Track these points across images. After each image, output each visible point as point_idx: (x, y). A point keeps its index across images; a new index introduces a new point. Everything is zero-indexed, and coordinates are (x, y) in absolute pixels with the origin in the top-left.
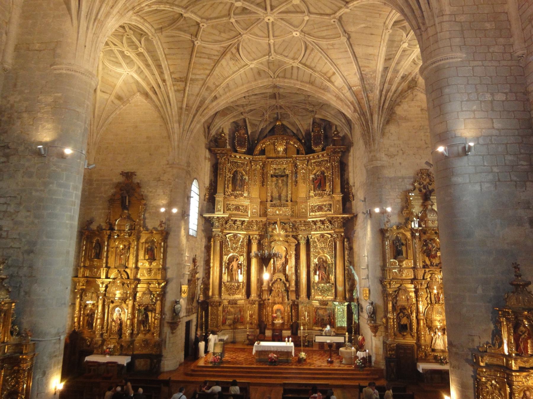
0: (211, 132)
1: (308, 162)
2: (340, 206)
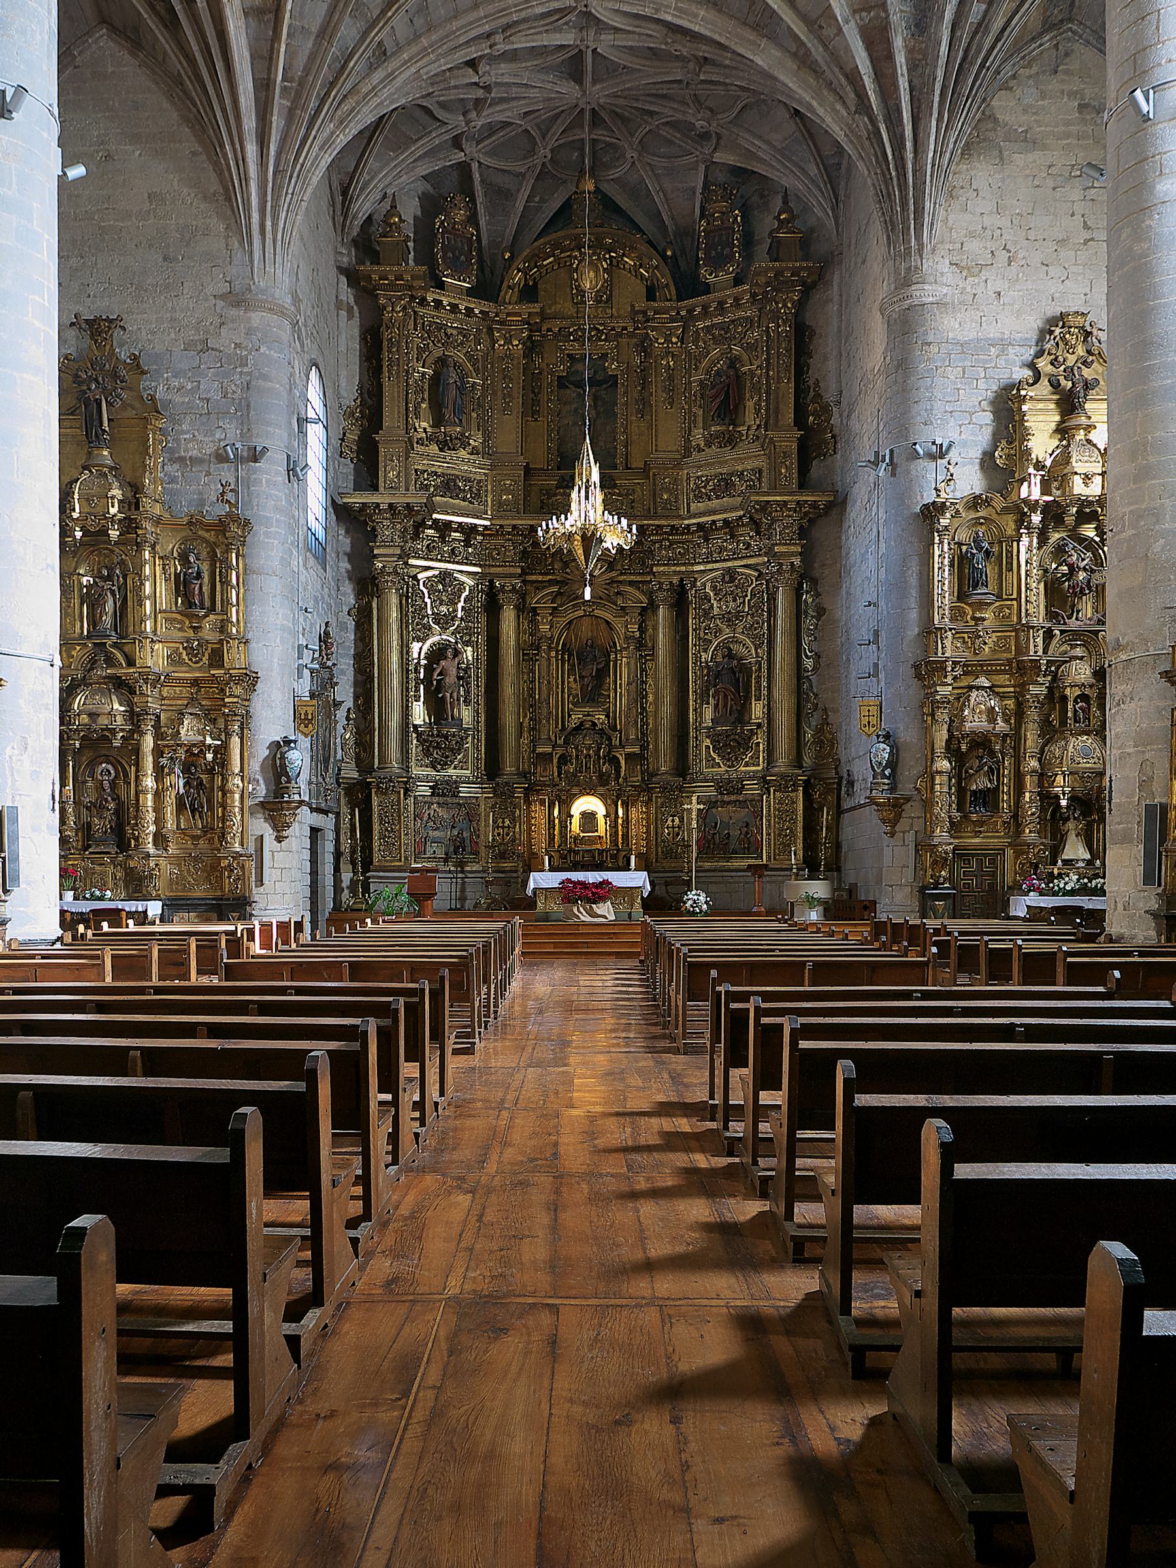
0: (355, 207)
1: (685, 329)
2: (789, 470)
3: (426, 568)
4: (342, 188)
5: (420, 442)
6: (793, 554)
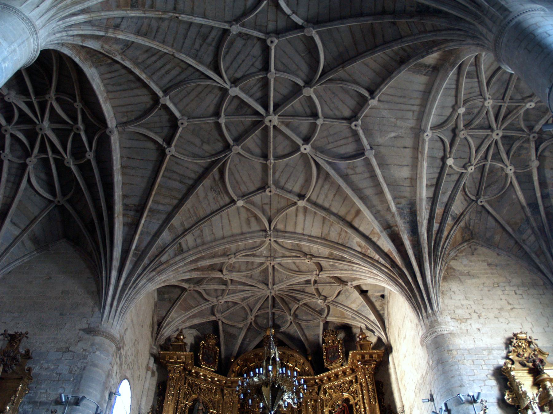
0: (163, 331)
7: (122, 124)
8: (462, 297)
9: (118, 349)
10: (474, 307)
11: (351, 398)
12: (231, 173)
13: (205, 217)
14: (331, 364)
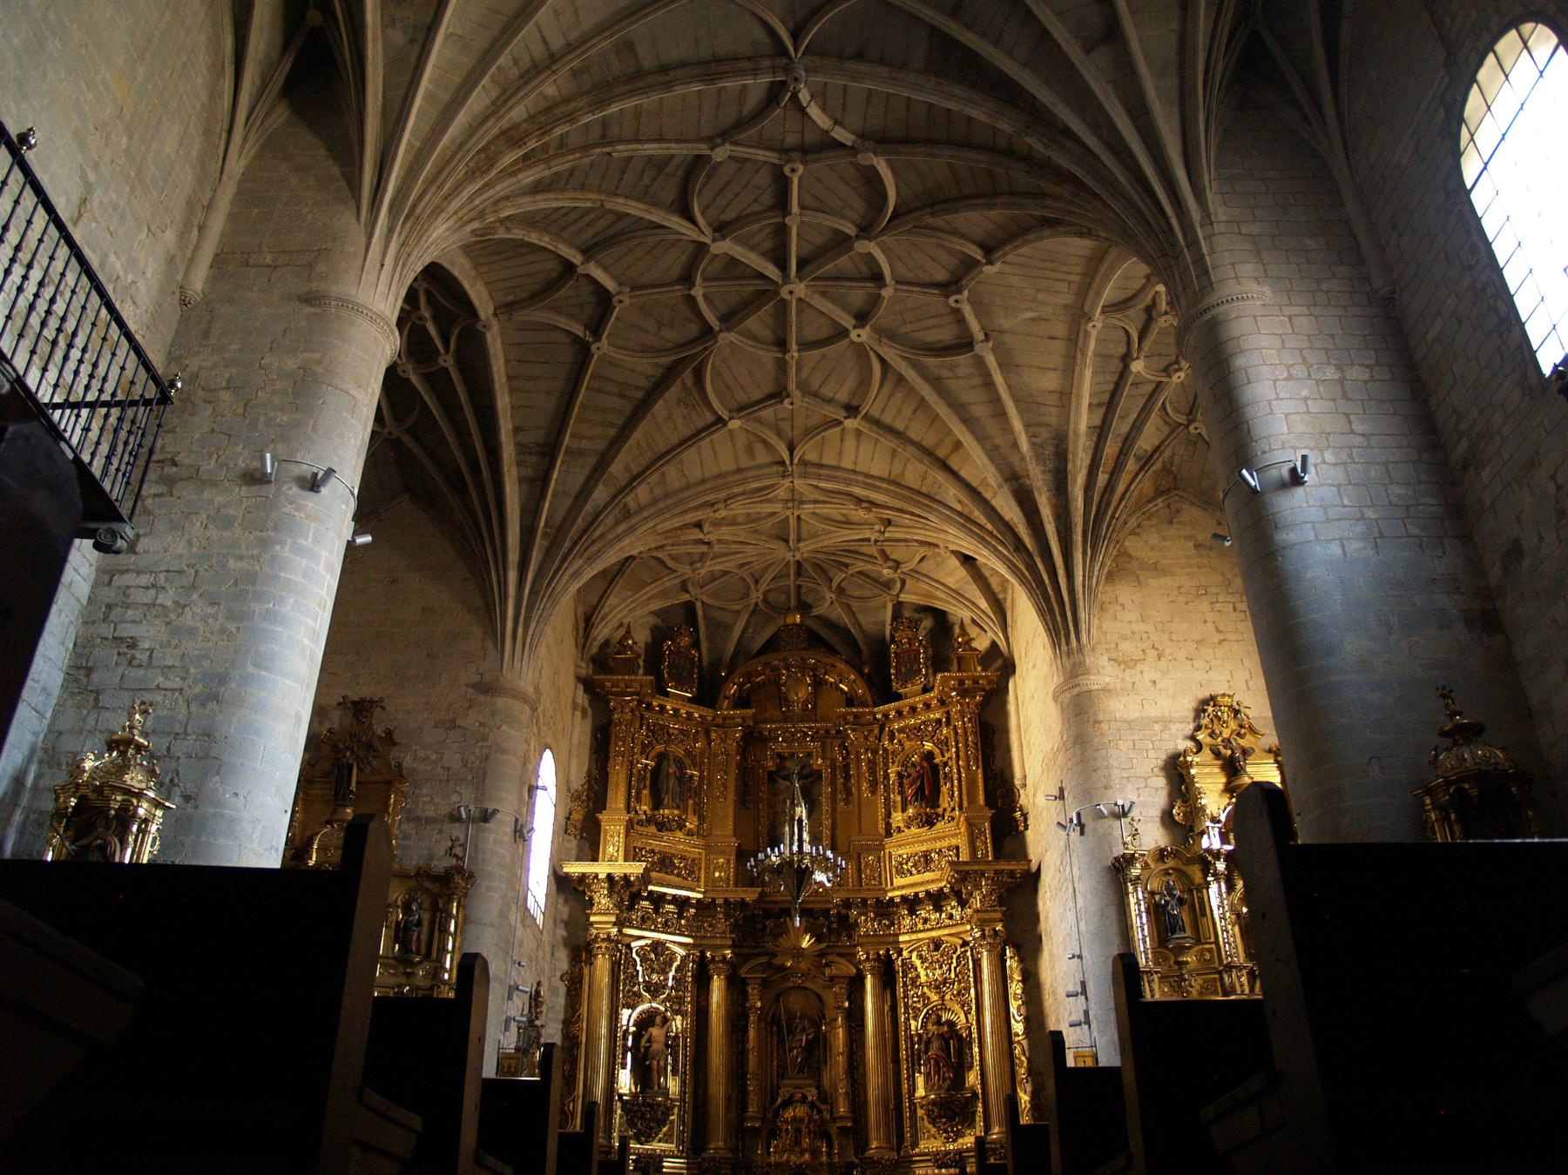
0: (594, 633)
3: (642, 938)
4: (587, 622)
5: (640, 823)
6: (995, 921)
7: (505, 309)
8: (1135, 616)
9: (534, 710)
10: (1154, 638)
11: (937, 751)
12: (717, 373)
13: (669, 452)
14: (904, 685)
